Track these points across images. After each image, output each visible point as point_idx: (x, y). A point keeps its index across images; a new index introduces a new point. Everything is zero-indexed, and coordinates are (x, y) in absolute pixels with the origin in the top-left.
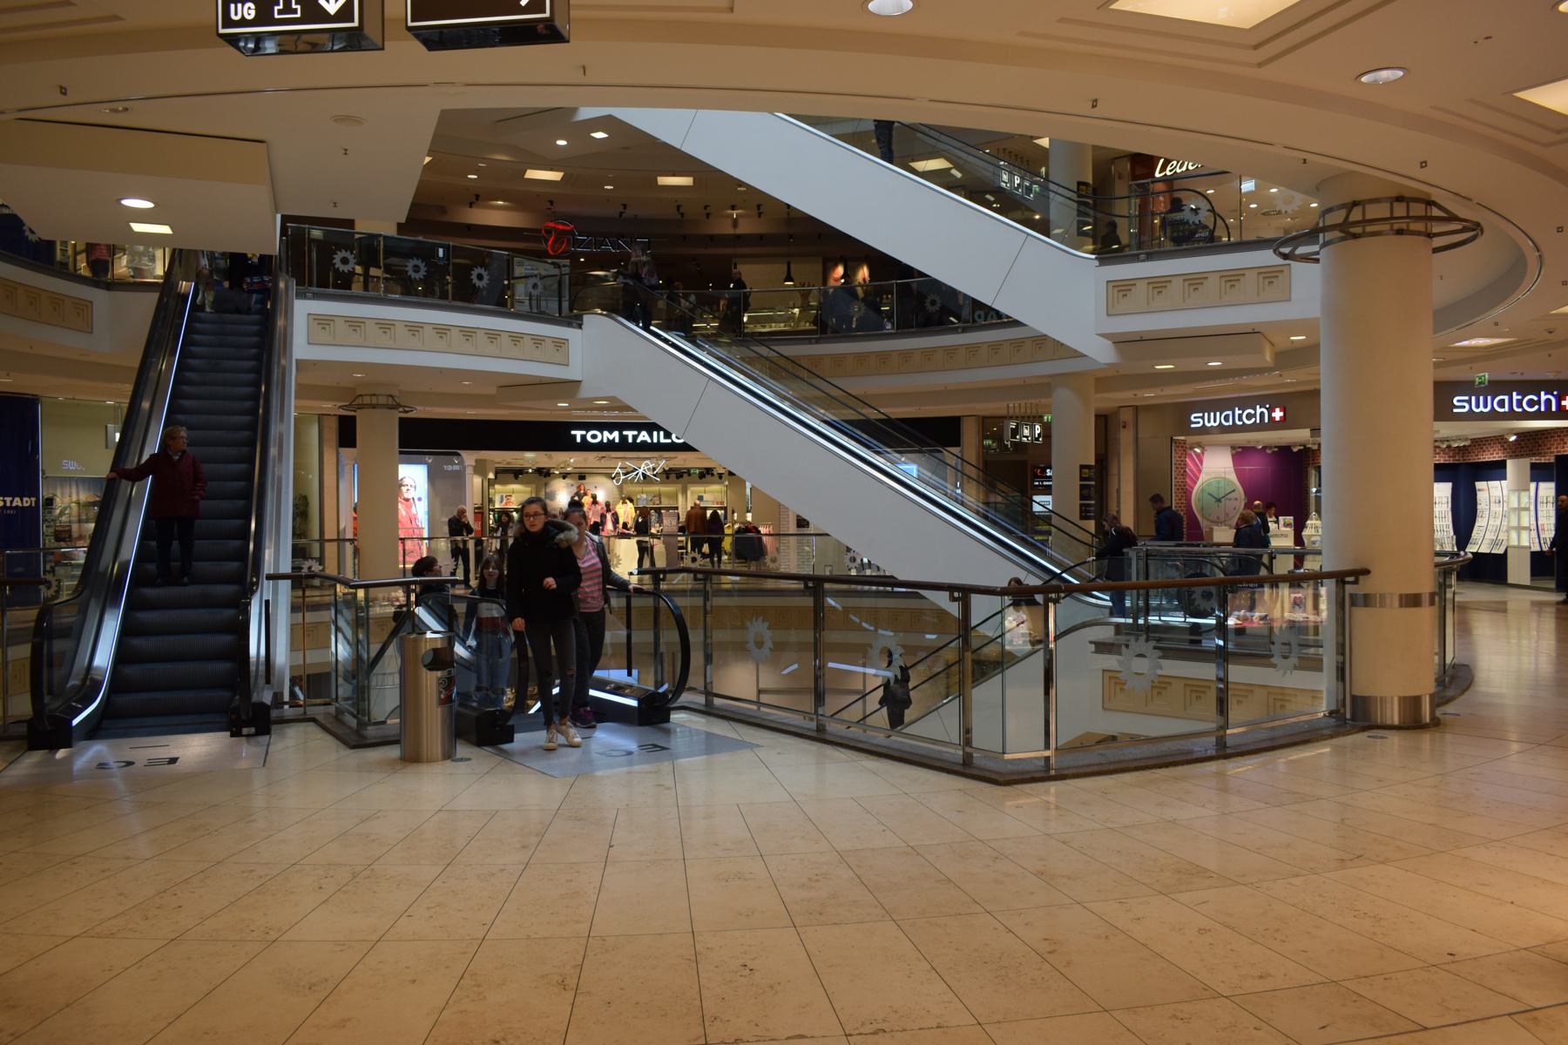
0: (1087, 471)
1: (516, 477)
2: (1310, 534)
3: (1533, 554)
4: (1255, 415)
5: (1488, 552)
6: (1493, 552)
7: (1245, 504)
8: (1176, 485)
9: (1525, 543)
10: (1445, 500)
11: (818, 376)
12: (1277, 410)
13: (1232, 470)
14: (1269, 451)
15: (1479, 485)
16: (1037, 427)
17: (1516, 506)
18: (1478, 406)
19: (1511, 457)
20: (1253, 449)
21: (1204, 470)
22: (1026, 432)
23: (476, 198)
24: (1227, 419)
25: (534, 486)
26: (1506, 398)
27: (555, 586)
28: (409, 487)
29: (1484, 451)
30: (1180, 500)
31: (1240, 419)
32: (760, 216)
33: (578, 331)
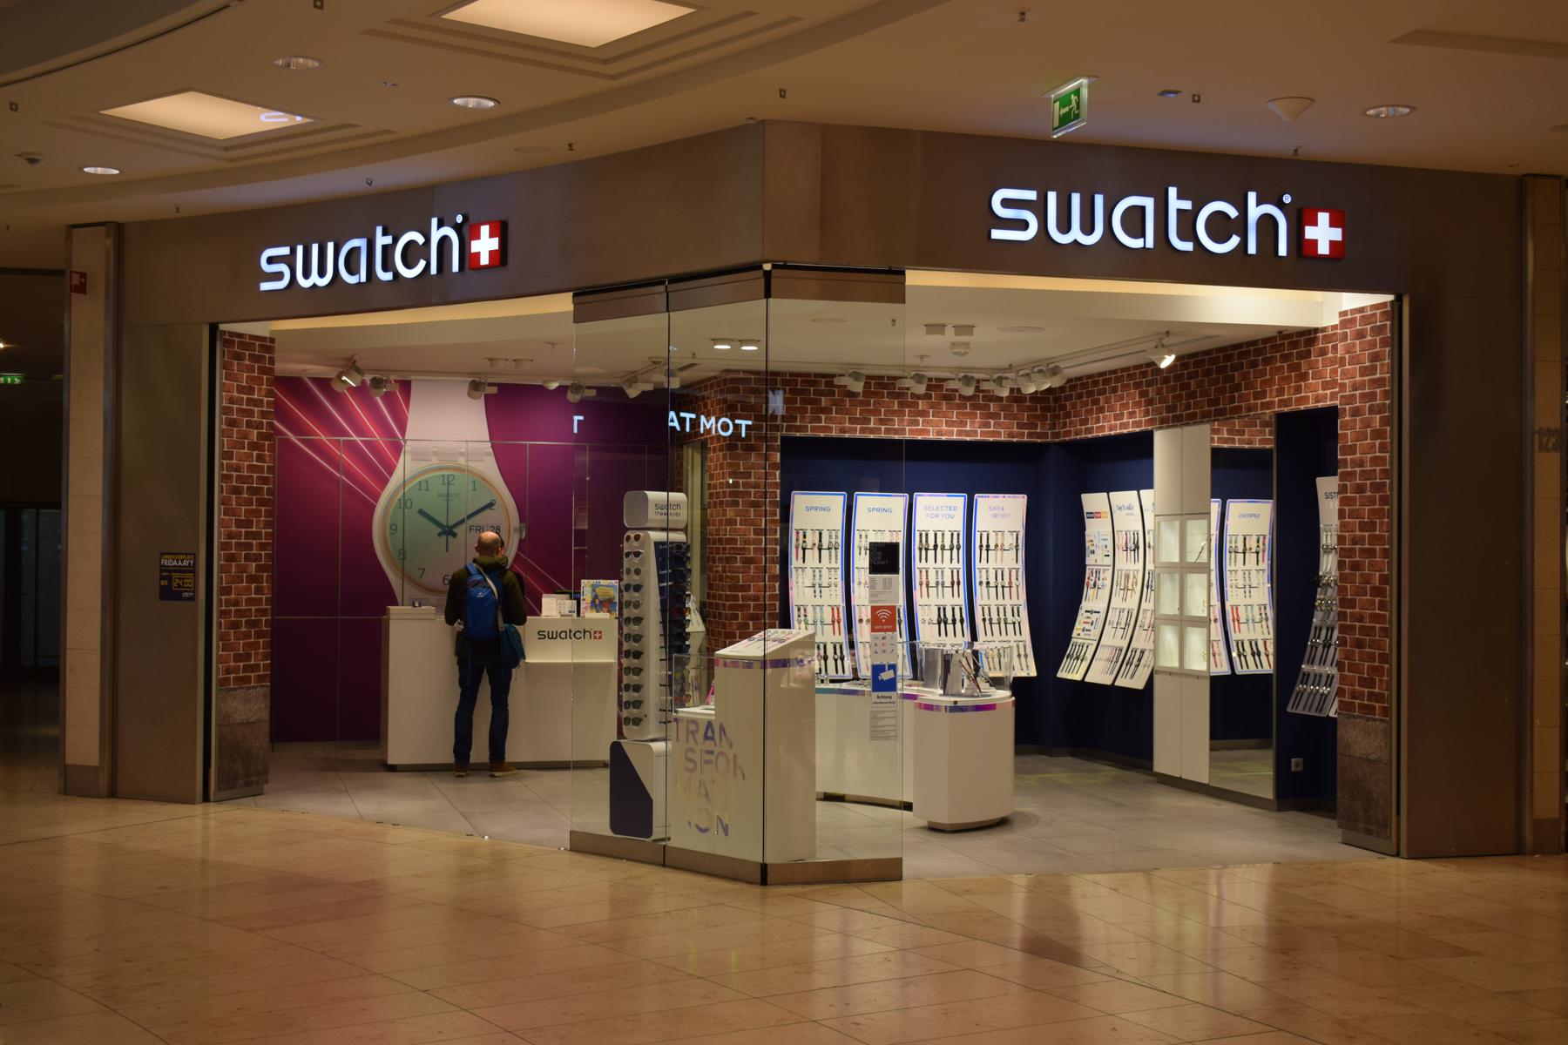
3: (1217, 682)
5: (1109, 682)
6: (1119, 683)
7: (521, 542)
9: (1197, 663)
10: (1009, 540)
15: (1092, 501)
17: (1176, 559)
18: (1065, 227)
19: (1165, 423)
21: (408, 447)
26: (1148, 203)
27: (1061, 674)
29: (1101, 410)
30: (1369, 682)
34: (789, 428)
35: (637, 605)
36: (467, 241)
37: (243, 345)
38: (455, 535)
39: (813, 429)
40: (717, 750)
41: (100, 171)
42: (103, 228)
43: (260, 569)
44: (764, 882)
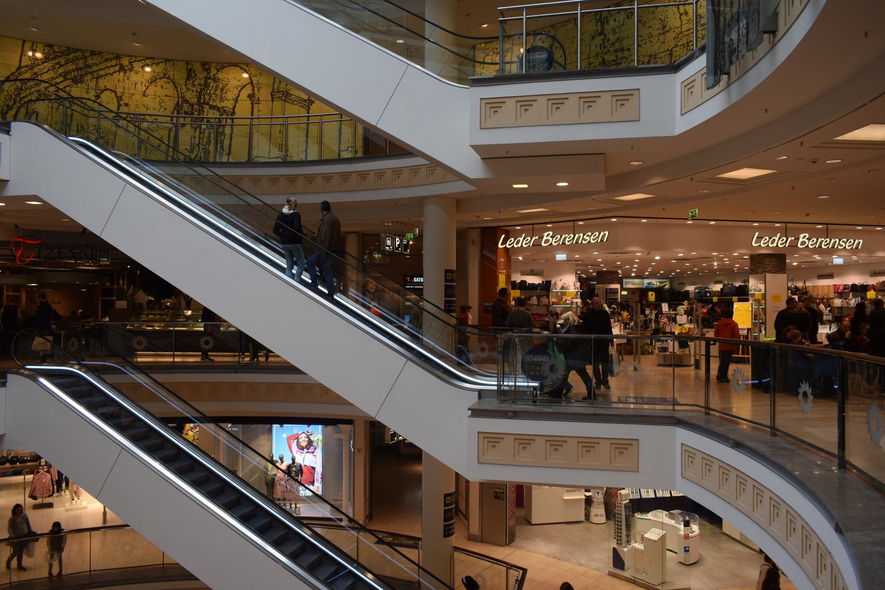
11: (248, 193)
16: (397, 239)
42: (477, 229)
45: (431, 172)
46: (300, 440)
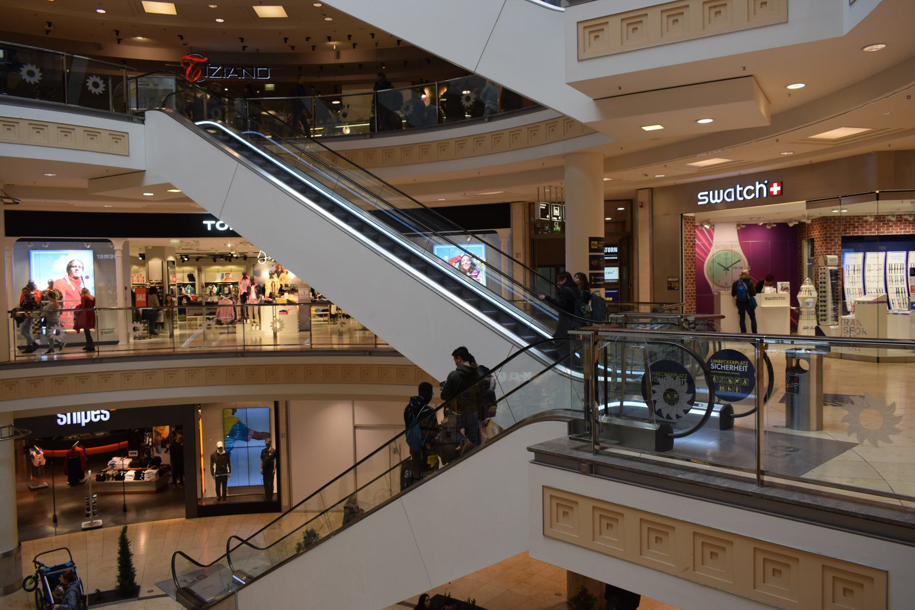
0: (596, 243)
1: (215, 261)
2: (804, 296)
4: (754, 191)
8: (686, 256)
12: (775, 185)
13: (738, 243)
14: (768, 227)
20: (755, 226)
21: (714, 244)
22: (556, 212)
23: (120, 36)
24: (729, 195)
25: (245, 266)
28: (78, 268)
30: (690, 269)
31: (741, 195)
32: (354, 47)
33: (140, 126)
34: (845, 233)
35: (824, 287)
36: (768, 188)
37: (689, 219)
38: (728, 270)
39: (853, 233)
40: (856, 327)
41: (659, 176)
42: (647, 190)
43: (694, 281)
44: (878, 362)
45: (533, 133)
46: (462, 263)
